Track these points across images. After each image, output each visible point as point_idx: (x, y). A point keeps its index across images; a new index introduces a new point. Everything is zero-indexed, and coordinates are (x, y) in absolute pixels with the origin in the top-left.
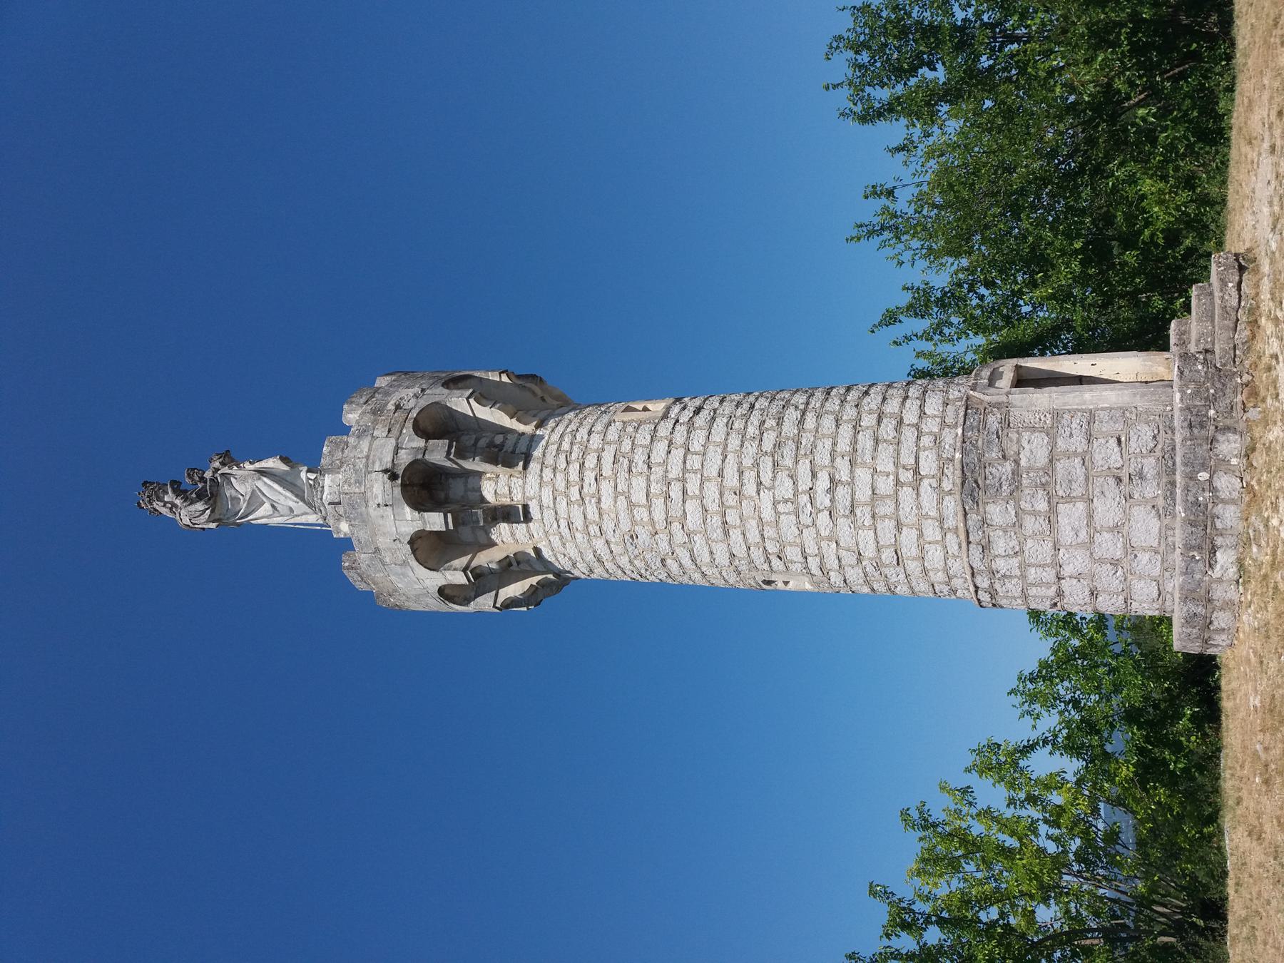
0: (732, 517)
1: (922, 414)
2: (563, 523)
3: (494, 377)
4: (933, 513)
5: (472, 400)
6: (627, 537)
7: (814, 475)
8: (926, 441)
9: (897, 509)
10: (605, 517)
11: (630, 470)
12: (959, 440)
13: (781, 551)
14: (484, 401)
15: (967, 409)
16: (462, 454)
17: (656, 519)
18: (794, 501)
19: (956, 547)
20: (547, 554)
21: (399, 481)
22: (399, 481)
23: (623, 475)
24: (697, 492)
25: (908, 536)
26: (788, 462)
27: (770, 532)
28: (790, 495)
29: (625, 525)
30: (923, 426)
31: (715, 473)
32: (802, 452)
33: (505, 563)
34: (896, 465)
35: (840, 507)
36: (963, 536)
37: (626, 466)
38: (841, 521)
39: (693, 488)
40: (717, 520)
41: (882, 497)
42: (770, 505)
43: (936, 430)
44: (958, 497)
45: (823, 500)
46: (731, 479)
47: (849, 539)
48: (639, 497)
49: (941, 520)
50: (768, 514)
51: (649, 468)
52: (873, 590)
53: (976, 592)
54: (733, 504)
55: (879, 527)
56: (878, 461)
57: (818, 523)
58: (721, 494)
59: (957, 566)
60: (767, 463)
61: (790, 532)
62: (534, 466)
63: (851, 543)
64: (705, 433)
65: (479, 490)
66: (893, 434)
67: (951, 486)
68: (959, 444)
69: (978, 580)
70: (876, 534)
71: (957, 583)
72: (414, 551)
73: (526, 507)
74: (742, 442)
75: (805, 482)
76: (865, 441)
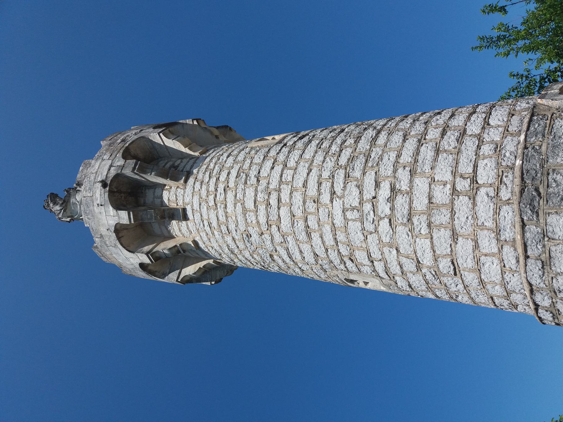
0: (312, 222)
1: (486, 123)
2: (206, 223)
3: (189, 122)
4: (490, 224)
5: (161, 134)
6: (245, 236)
7: (377, 185)
8: (486, 149)
9: (452, 218)
10: (229, 219)
11: (246, 183)
12: (521, 146)
13: (351, 254)
14: (171, 136)
15: (532, 115)
16: (143, 170)
17: (261, 222)
18: (359, 209)
19: (514, 261)
20: (202, 245)
21: (108, 189)
22: (108, 189)
23: (241, 186)
24: (288, 200)
25: (464, 248)
26: (357, 174)
27: (341, 237)
28: (356, 203)
29: (242, 227)
30: (485, 136)
31: (301, 185)
32: (370, 164)
33: (174, 250)
34: (454, 174)
35: (398, 215)
36: (520, 250)
37: (243, 180)
38: (400, 229)
39: (285, 197)
40: (301, 225)
41: (438, 207)
42: (340, 212)
43: (497, 138)
44: (516, 206)
45: (384, 208)
46: (312, 191)
47: (407, 247)
48: (250, 204)
49: (498, 232)
50: (339, 220)
51: (258, 181)
52: (437, 296)
53: (536, 310)
54: (313, 210)
55: (435, 236)
56: (437, 170)
57: (380, 229)
58: (304, 202)
59: (515, 282)
60: (340, 175)
61: (357, 237)
62: (191, 180)
63: (410, 251)
64: (300, 152)
65: (161, 197)
66: (454, 144)
67: (509, 195)
68: (520, 151)
69: (538, 298)
70: (432, 243)
71: (516, 298)
72: (119, 238)
73: (184, 210)
74: (325, 158)
75: (368, 194)
76: (427, 152)
